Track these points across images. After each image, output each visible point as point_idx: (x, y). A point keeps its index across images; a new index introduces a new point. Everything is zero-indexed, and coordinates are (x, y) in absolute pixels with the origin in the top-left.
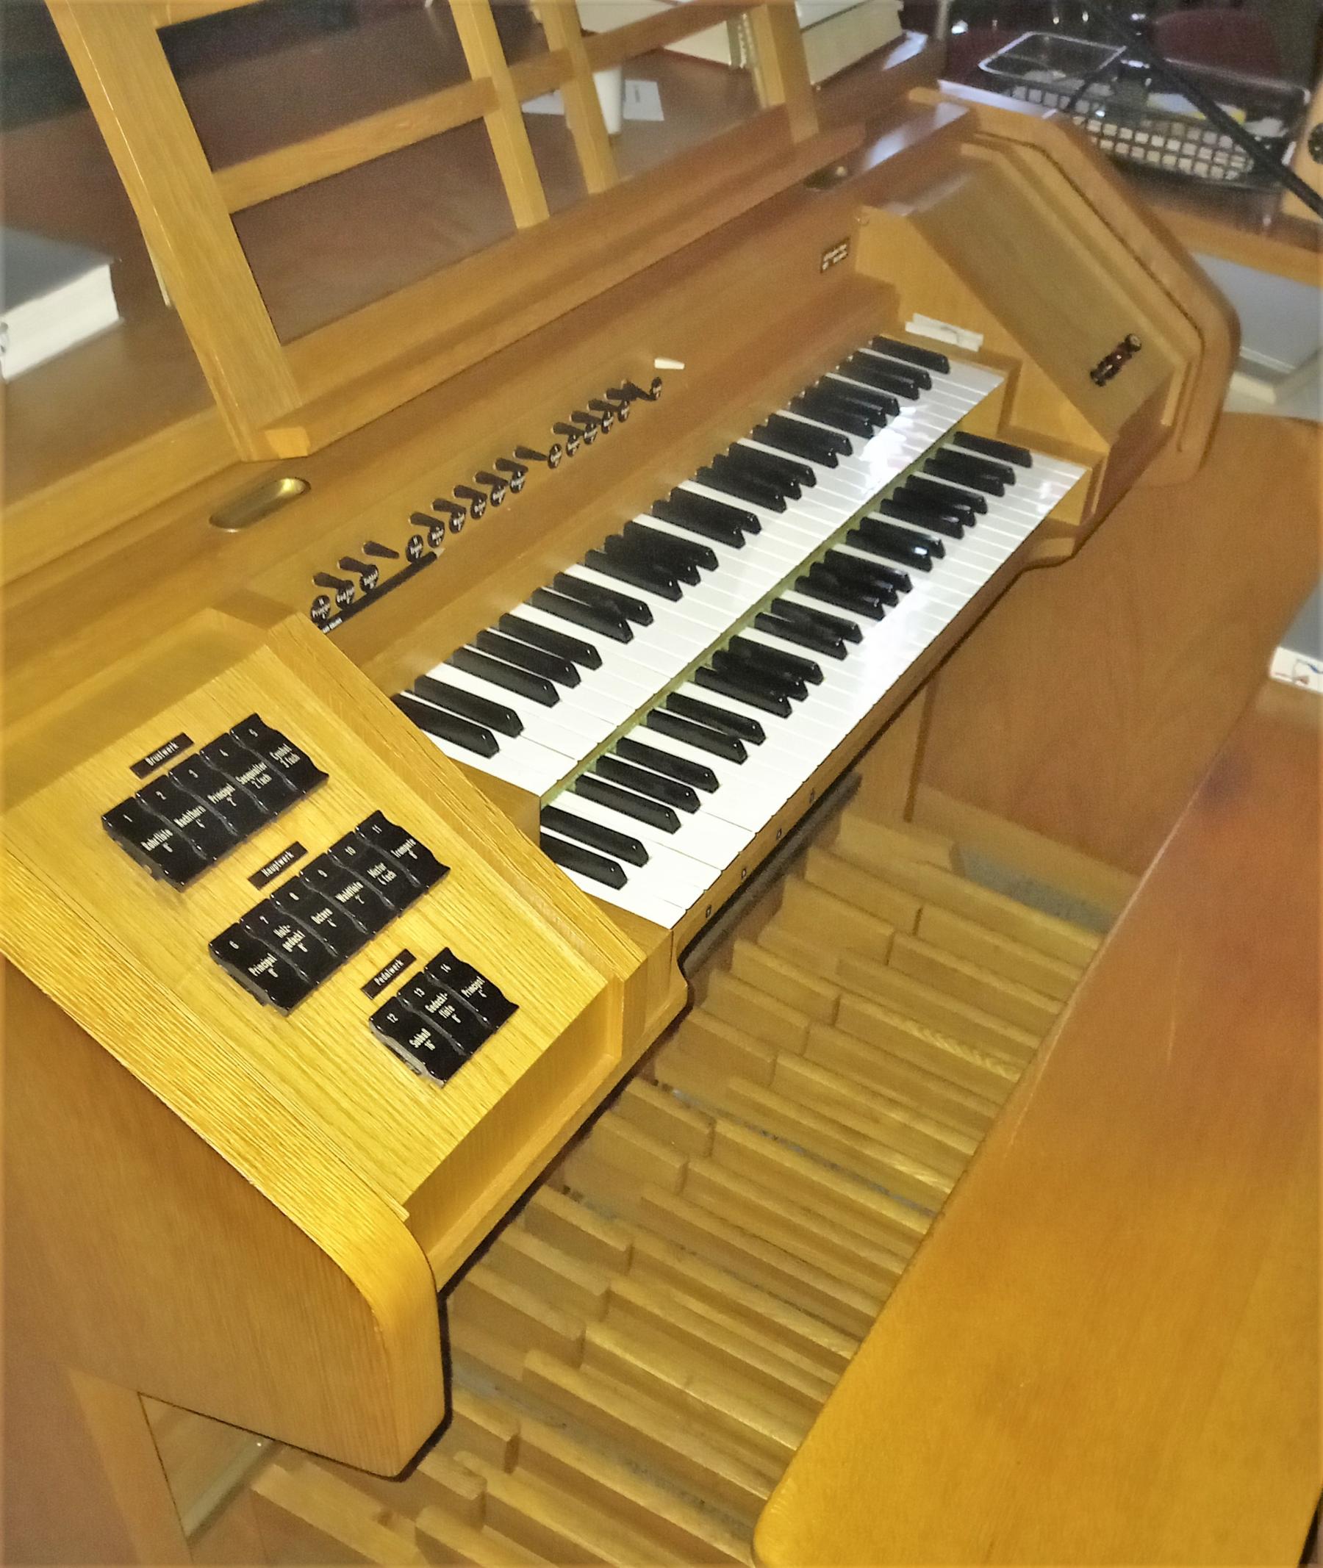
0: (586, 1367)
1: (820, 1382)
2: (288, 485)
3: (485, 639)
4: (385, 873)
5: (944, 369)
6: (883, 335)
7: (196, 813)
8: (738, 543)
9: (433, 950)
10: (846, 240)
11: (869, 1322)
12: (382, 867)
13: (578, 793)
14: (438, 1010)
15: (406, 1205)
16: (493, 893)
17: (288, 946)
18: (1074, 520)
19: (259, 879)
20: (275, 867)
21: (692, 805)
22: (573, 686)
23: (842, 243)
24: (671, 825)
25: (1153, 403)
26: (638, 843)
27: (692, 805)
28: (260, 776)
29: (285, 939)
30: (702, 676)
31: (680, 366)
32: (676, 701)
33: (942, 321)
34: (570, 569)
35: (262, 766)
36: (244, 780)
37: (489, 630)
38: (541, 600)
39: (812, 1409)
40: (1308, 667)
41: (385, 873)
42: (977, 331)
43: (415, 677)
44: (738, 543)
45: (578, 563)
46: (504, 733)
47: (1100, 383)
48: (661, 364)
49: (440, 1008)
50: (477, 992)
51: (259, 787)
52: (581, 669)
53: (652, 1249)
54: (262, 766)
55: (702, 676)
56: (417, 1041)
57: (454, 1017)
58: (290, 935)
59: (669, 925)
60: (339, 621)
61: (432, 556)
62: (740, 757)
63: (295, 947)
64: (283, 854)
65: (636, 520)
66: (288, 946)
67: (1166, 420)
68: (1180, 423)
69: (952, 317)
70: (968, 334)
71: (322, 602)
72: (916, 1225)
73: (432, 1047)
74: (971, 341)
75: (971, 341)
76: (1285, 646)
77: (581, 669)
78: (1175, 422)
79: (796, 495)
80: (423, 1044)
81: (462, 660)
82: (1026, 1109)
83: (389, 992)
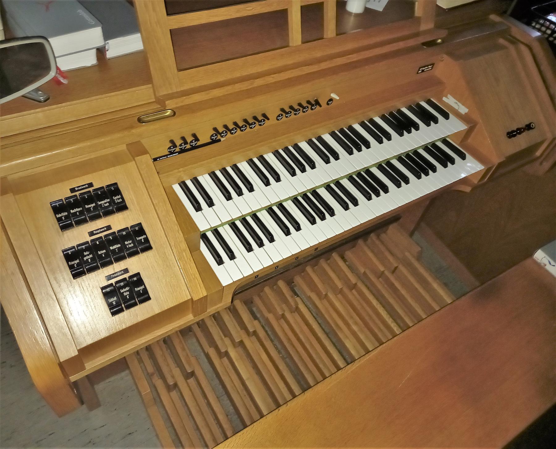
0: (354, 291)
1: (251, 417)
2: (439, 41)
3: (391, 114)
4: (130, 244)
5: (446, 116)
6: (432, 99)
7: (79, 209)
8: (428, 125)
9: (135, 272)
10: (433, 64)
11: (310, 387)
12: (131, 242)
13: (349, 180)
14: (124, 292)
15: (79, 351)
16: (167, 258)
17: (85, 259)
18: (476, 182)
19: (91, 234)
20: (99, 231)
21: (427, 174)
22: (401, 136)
23: (431, 65)
24: (419, 177)
25: (536, 146)
26: (387, 187)
27: (427, 174)
28: (106, 203)
29: (86, 256)
30: (400, 159)
31: (338, 98)
32: (389, 163)
33: (456, 100)
34: (422, 102)
35: (108, 200)
36: (100, 203)
37: (386, 114)
38: (410, 109)
39: (305, 387)
40: (548, 261)
41: (130, 244)
42: (467, 107)
43: (428, 99)
44: (428, 125)
45: (406, 108)
46: (356, 149)
47: (510, 137)
48: (333, 96)
49: (125, 292)
50: (140, 290)
51: (103, 206)
52: (413, 129)
53: (262, 334)
54: (108, 200)
55: (400, 159)
56: (111, 300)
57: (128, 296)
58: (88, 255)
59: (224, 284)
60: (177, 154)
61: (219, 140)
62: (399, 186)
63: (87, 260)
64: (103, 228)
65: (420, 103)
66: (85, 259)
67: (538, 153)
68: (544, 156)
69: (460, 99)
70: (463, 107)
71: (280, 115)
72: (396, 330)
73: (141, 292)
74: (463, 110)
75: (463, 110)
76: (543, 251)
77: (413, 129)
78: (542, 155)
79: (409, 132)
80: (112, 302)
81: (383, 118)
82: (338, 381)
83: (113, 281)
